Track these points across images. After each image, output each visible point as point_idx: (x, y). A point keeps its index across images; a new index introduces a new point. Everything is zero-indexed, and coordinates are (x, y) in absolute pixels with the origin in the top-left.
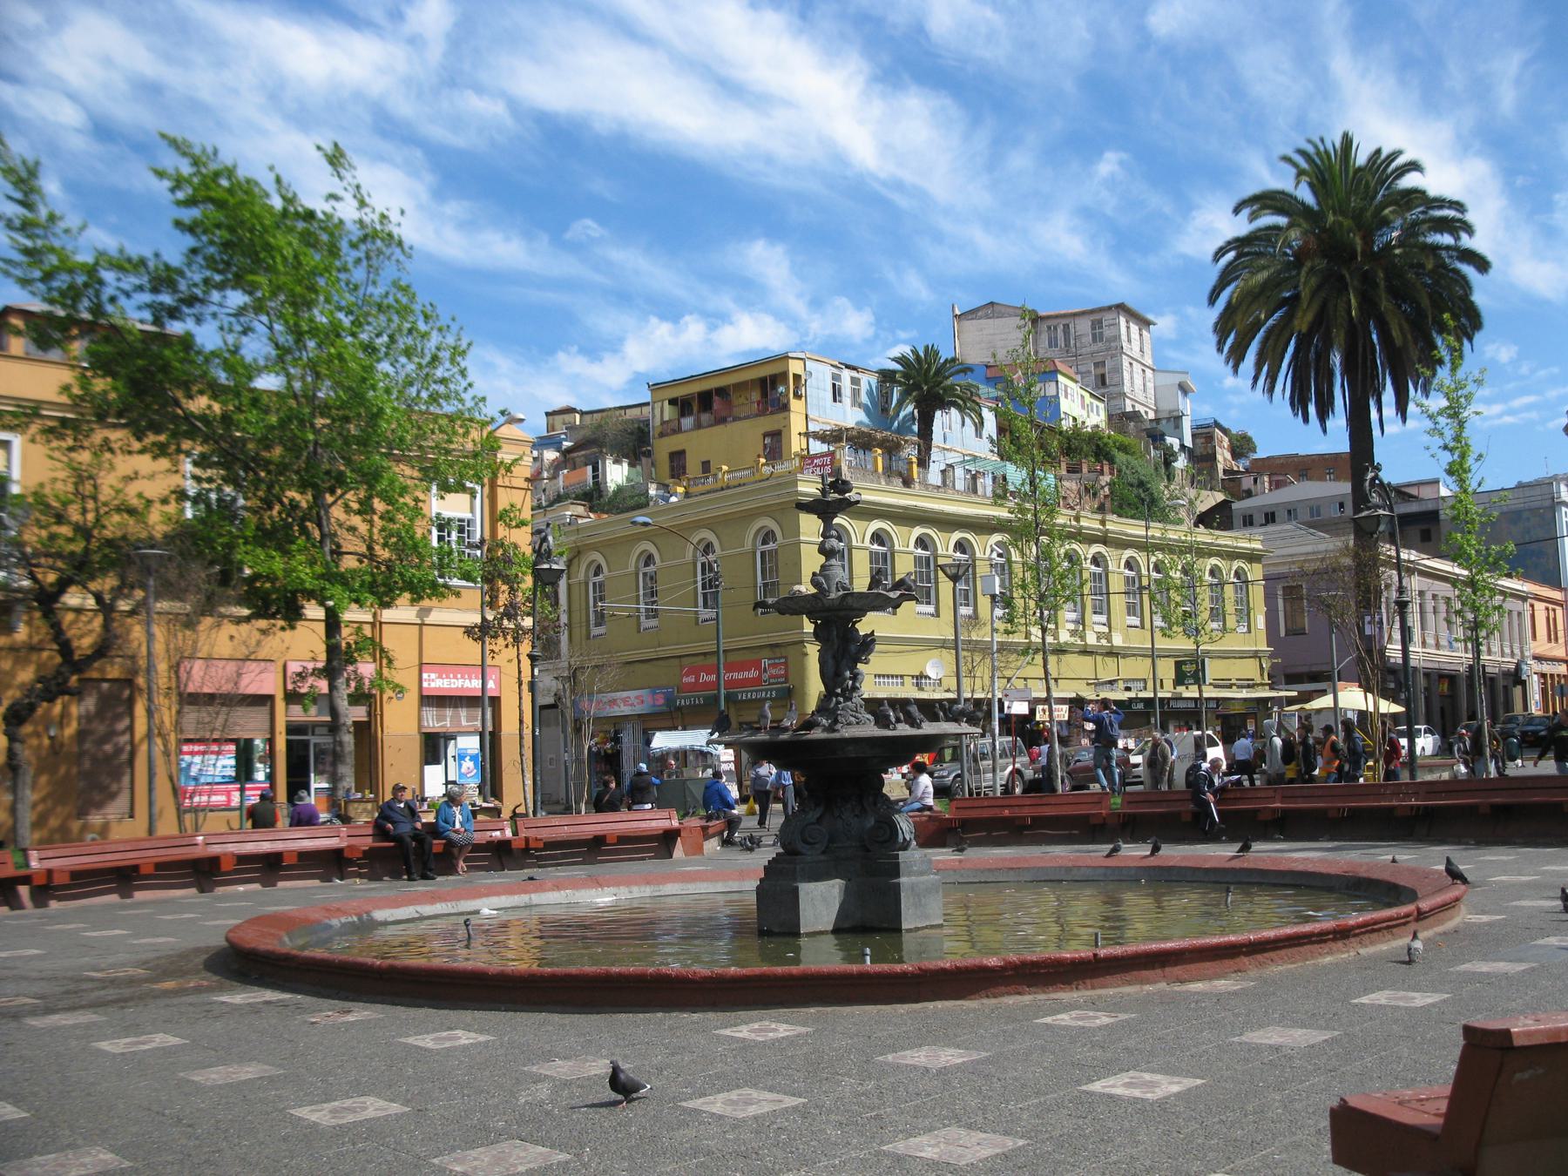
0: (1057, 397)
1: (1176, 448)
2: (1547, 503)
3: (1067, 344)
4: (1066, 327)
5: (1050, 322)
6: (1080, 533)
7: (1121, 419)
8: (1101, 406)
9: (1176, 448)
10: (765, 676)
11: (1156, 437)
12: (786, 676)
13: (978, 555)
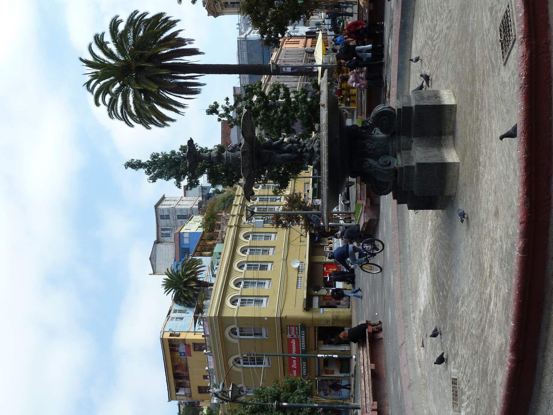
0: (190, 233)
1: (214, 189)
2: (245, 43)
3: (169, 230)
4: (162, 230)
5: (160, 236)
6: (242, 205)
7: (201, 209)
8: (195, 217)
9: (214, 189)
10: (295, 336)
11: (209, 196)
12: (295, 326)
13: (248, 245)
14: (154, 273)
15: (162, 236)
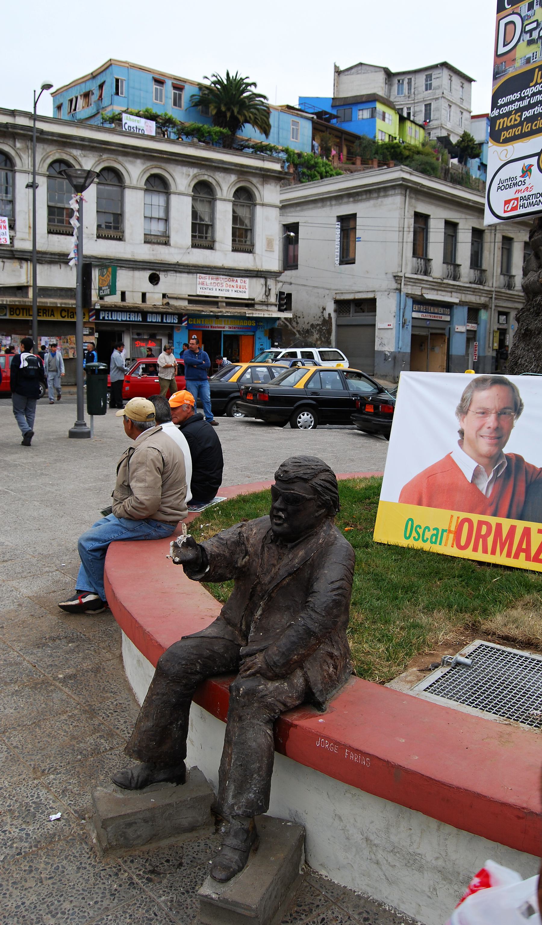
14: (338, 72)
15: (399, 81)
